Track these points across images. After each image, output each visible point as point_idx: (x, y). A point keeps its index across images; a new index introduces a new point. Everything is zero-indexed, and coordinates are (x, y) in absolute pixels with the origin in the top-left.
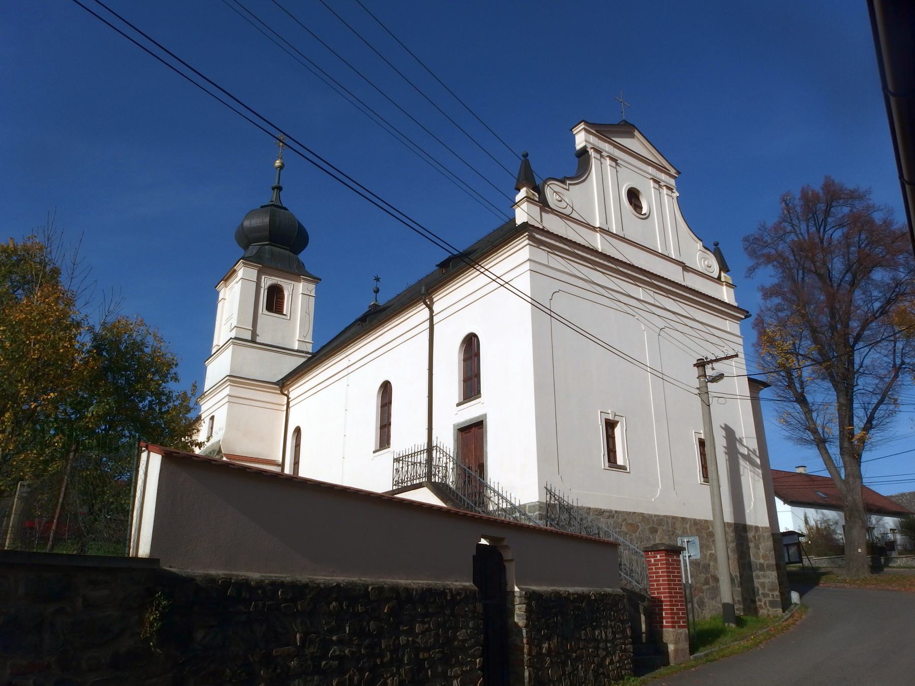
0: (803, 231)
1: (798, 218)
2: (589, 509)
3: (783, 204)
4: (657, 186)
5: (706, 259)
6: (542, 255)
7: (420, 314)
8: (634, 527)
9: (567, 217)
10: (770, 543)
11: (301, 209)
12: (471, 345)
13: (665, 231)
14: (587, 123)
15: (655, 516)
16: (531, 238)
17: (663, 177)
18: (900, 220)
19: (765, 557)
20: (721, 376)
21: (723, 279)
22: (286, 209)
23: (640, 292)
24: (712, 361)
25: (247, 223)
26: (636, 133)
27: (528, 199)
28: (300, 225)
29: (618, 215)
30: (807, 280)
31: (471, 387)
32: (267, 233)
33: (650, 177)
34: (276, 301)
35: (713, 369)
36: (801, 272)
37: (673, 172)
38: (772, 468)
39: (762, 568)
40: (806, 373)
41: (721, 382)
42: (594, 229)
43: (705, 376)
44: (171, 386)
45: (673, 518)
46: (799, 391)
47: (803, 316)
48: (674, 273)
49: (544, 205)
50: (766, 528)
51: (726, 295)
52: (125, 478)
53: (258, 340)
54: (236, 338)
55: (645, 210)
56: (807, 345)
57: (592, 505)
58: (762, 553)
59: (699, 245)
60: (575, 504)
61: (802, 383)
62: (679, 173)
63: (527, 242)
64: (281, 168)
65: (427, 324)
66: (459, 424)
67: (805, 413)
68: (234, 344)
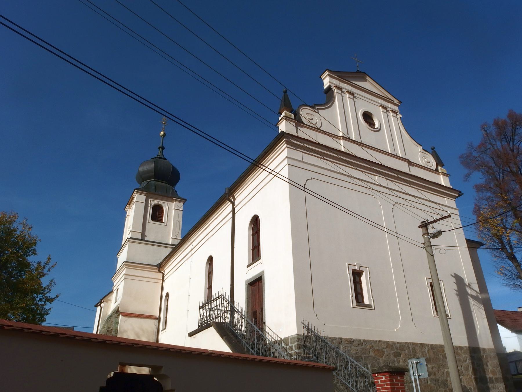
0: (499, 147)
1: (494, 140)
2: (341, 339)
3: (483, 132)
4: (385, 111)
5: (425, 158)
6: (298, 154)
7: (227, 208)
8: (380, 352)
9: (318, 130)
10: (496, 361)
11: (174, 158)
12: (255, 222)
13: (392, 136)
14: (330, 71)
15: (398, 343)
16: (288, 143)
17: (389, 105)
19: (493, 372)
20: (440, 233)
21: (440, 171)
22: (166, 159)
23: (377, 179)
24: (432, 222)
25: (141, 169)
26: (368, 78)
27: (287, 118)
28: (173, 168)
29: (356, 129)
30: (506, 178)
32: (153, 174)
33: (379, 105)
34: (157, 214)
35: (433, 228)
36: (501, 175)
37: (396, 101)
38: (495, 308)
39: (497, 380)
40: (514, 239)
41: (440, 238)
42: (337, 137)
43: (428, 234)
44: (32, 259)
45: (414, 344)
46: (510, 251)
47: (506, 201)
48: (403, 167)
49: (298, 122)
50: (492, 349)
51: (443, 180)
53: (146, 239)
54: (131, 238)
55: (377, 125)
56: (511, 221)
57: (344, 336)
58: (492, 369)
59: (420, 148)
60: (322, 335)
61: (511, 248)
62: (400, 102)
63: (285, 145)
64: (164, 136)
65: (230, 215)
66: (249, 280)
67: (516, 267)
68: (129, 241)
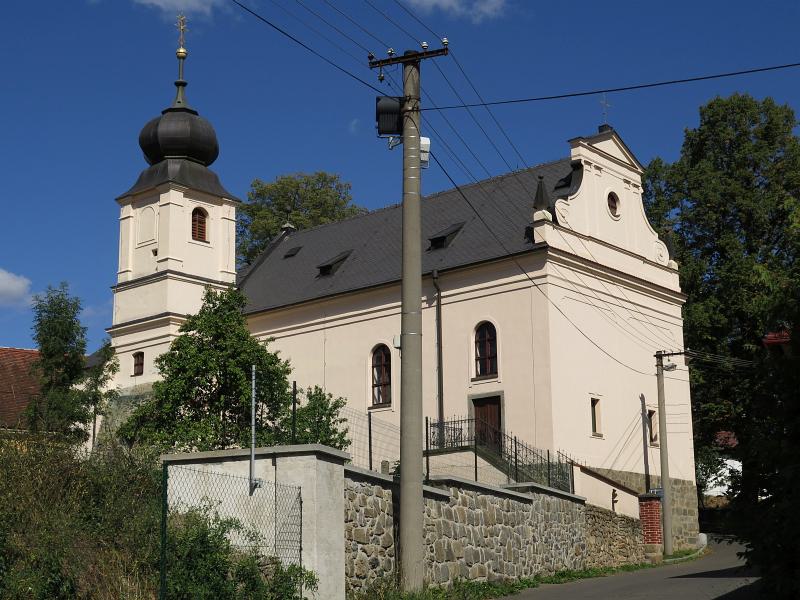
18: (260, 336)
31: (487, 364)
52: (673, 214)
